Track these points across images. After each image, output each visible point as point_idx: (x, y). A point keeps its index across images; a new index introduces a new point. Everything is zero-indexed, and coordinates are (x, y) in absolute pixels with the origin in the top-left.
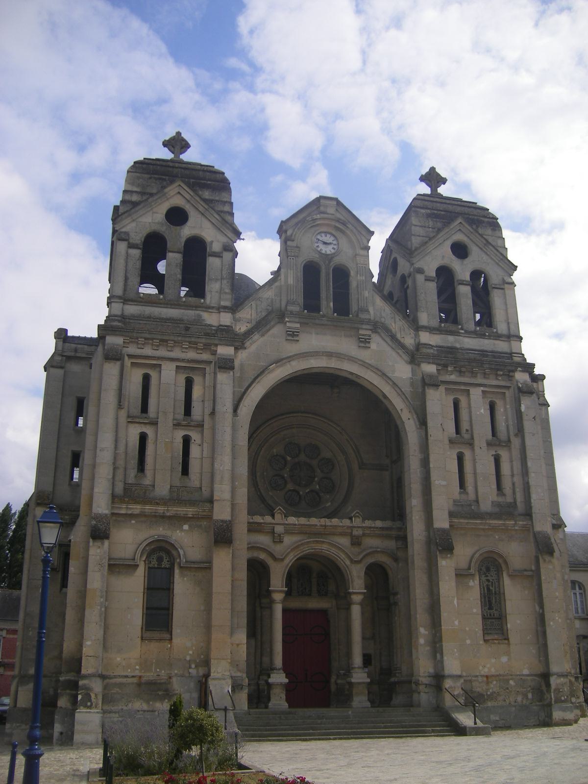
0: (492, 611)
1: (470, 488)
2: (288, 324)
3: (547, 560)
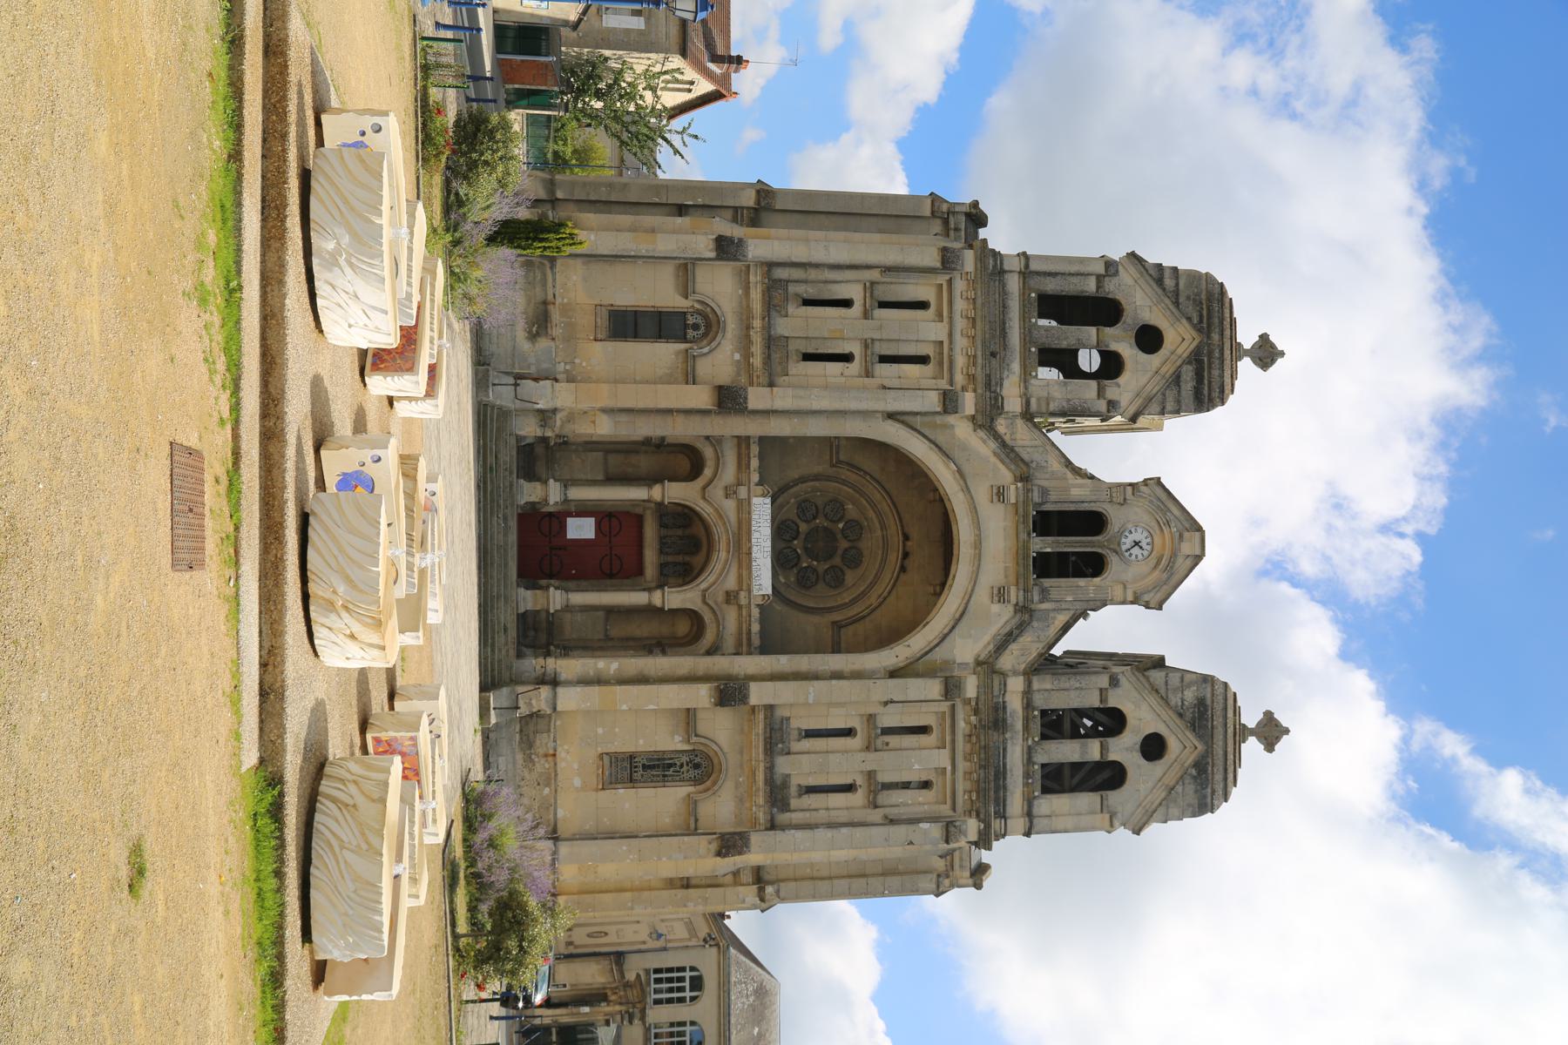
1: (808, 744)
2: (1013, 487)
3: (710, 846)
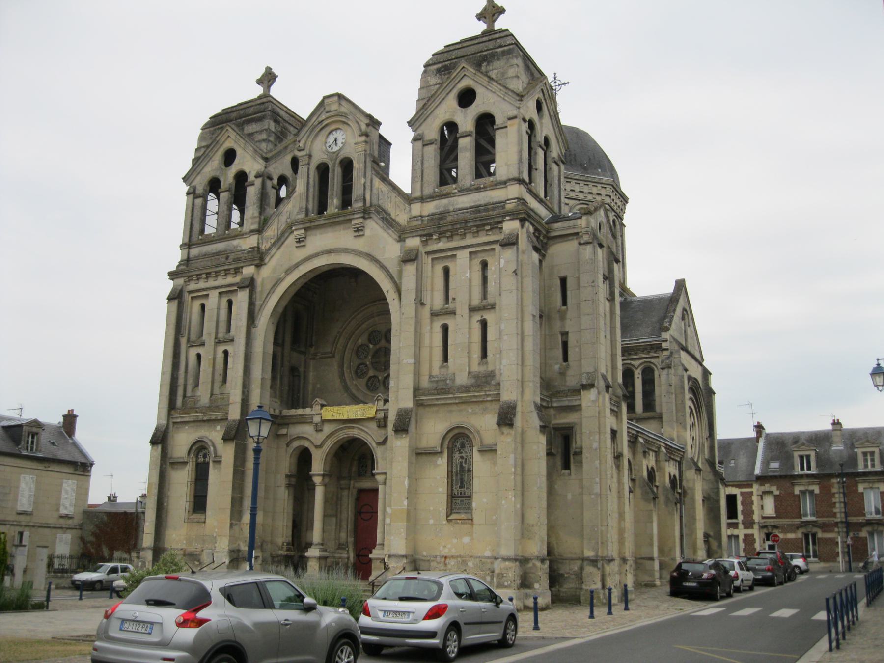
0: (462, 489)
